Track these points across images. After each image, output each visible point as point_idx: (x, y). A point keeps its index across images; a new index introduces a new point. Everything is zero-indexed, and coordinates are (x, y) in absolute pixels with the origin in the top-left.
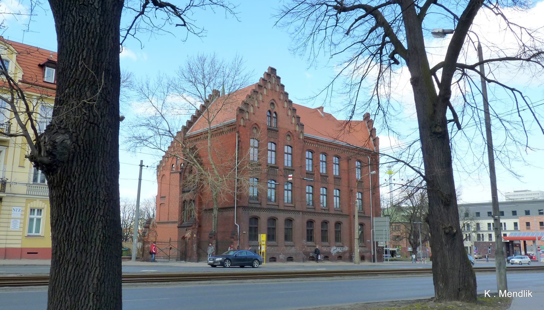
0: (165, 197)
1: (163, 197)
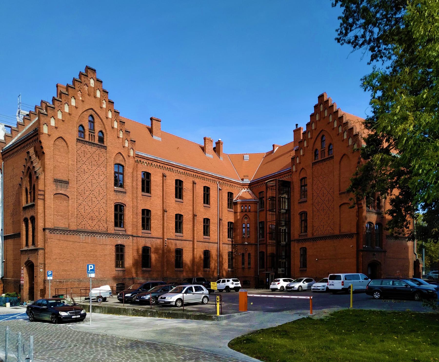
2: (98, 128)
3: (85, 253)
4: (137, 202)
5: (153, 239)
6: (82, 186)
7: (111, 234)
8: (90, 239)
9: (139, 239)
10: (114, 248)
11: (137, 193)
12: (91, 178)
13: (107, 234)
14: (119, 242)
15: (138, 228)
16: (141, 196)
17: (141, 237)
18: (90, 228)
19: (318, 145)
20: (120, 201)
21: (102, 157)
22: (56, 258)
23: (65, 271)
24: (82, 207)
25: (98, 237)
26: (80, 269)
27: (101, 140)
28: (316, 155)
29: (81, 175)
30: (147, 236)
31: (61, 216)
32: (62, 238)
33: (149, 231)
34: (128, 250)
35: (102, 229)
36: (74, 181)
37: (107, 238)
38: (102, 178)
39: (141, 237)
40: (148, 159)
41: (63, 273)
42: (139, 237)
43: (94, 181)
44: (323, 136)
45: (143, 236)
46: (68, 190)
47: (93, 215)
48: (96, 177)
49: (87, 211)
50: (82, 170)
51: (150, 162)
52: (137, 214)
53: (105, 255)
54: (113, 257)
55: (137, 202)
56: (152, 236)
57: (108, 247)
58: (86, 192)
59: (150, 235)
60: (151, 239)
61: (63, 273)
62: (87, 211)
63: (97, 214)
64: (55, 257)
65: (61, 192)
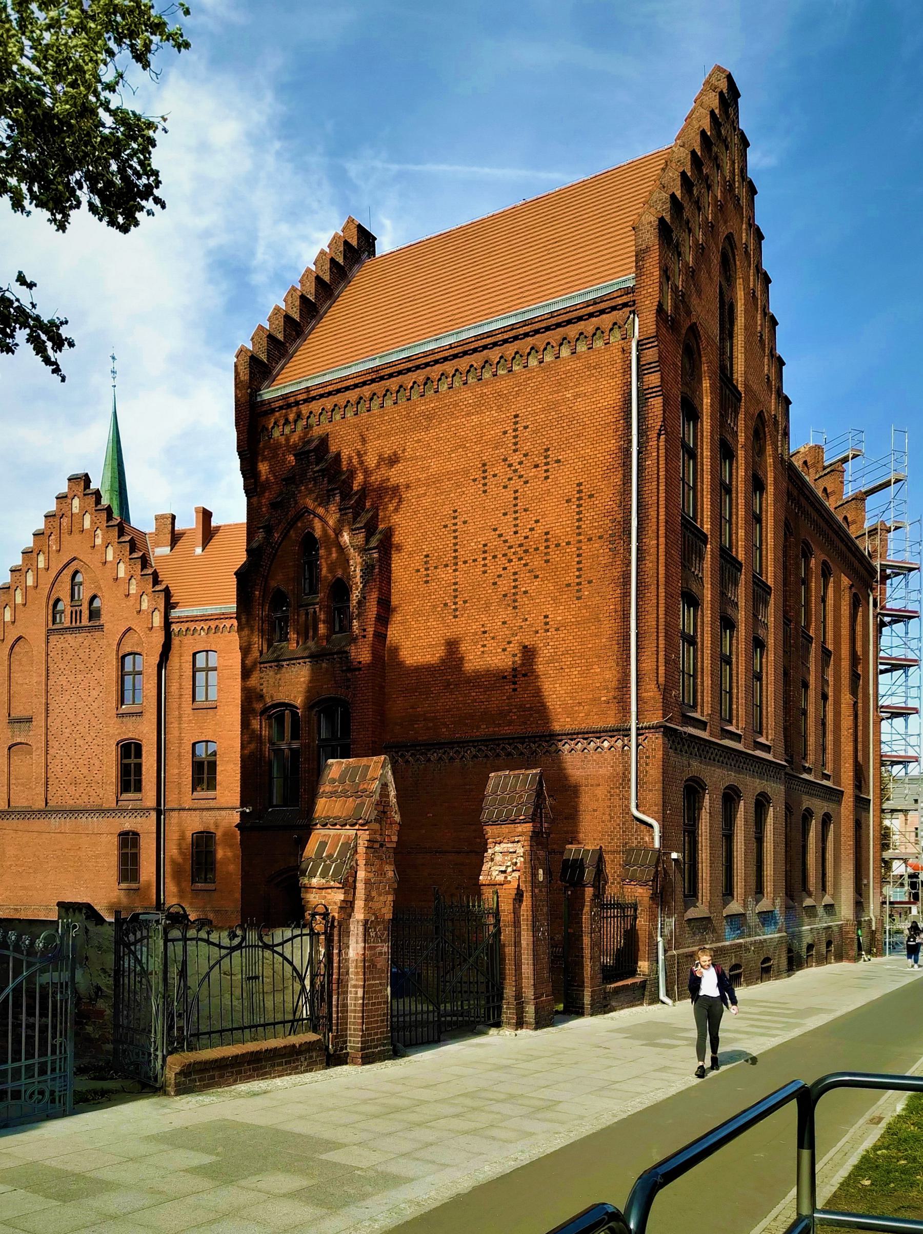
0: (29, 720)
1: (20, 721)
2: (84, 594)
3: (59, 853)
4: (180, 728)
5: (223, 813)
6: (59, 720)
7: (108, 810)
8: (68, 824)
9: (184, 814)
10: (115, 840)
11: (180, 707)
12: (74, 698)
13: (102, 811)
14: (127, 826)
15: (183, 790)
16: (191, 712)
17: (189, 809)
18: (72, 802)
19: (63, 591)
20: (130, 735)
21: (97, 649)
22: (11, 865)
23: (24, 888)
24: (57, 761)
25: (83, 820)
26: (50, 886)
27: (94, 614)
28: (55, 612)
29: (56, 698)
30: (207, 806)
31: (23, 785)
32: (21, 827)
33: (211, 794)
34: (148, 843)
35: (94, 801)
36: (41, 713)
37: (100, 819)
38: (94, 693)
39: (189, 809)
40: (205, 619)
41: (21, 893)
42: (184, 809)
43: (80, 705)
44: (76, 572)
45: (195, 806)
46: (31, 733)
47: (76, 773)
48: (84, 694)
49: (67, 768)
50: (59, 688)
51: (213, 624)
52: (179, 756)
53: (97, 856)
54: (114, 860)
55: (180, 728)
56: (218, 806)
57: (104, 839)
58: (64, 730)
59: (212, 804)
60: (217, 813)
61: (21, 893)
62: (67, 768)
63: (85, 771)
64: (9, 863)
65: (19, 740)
